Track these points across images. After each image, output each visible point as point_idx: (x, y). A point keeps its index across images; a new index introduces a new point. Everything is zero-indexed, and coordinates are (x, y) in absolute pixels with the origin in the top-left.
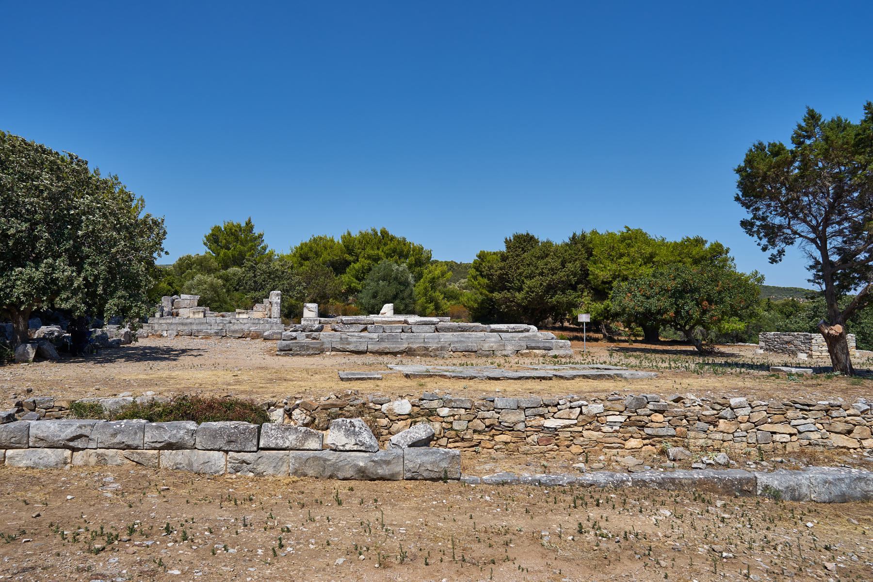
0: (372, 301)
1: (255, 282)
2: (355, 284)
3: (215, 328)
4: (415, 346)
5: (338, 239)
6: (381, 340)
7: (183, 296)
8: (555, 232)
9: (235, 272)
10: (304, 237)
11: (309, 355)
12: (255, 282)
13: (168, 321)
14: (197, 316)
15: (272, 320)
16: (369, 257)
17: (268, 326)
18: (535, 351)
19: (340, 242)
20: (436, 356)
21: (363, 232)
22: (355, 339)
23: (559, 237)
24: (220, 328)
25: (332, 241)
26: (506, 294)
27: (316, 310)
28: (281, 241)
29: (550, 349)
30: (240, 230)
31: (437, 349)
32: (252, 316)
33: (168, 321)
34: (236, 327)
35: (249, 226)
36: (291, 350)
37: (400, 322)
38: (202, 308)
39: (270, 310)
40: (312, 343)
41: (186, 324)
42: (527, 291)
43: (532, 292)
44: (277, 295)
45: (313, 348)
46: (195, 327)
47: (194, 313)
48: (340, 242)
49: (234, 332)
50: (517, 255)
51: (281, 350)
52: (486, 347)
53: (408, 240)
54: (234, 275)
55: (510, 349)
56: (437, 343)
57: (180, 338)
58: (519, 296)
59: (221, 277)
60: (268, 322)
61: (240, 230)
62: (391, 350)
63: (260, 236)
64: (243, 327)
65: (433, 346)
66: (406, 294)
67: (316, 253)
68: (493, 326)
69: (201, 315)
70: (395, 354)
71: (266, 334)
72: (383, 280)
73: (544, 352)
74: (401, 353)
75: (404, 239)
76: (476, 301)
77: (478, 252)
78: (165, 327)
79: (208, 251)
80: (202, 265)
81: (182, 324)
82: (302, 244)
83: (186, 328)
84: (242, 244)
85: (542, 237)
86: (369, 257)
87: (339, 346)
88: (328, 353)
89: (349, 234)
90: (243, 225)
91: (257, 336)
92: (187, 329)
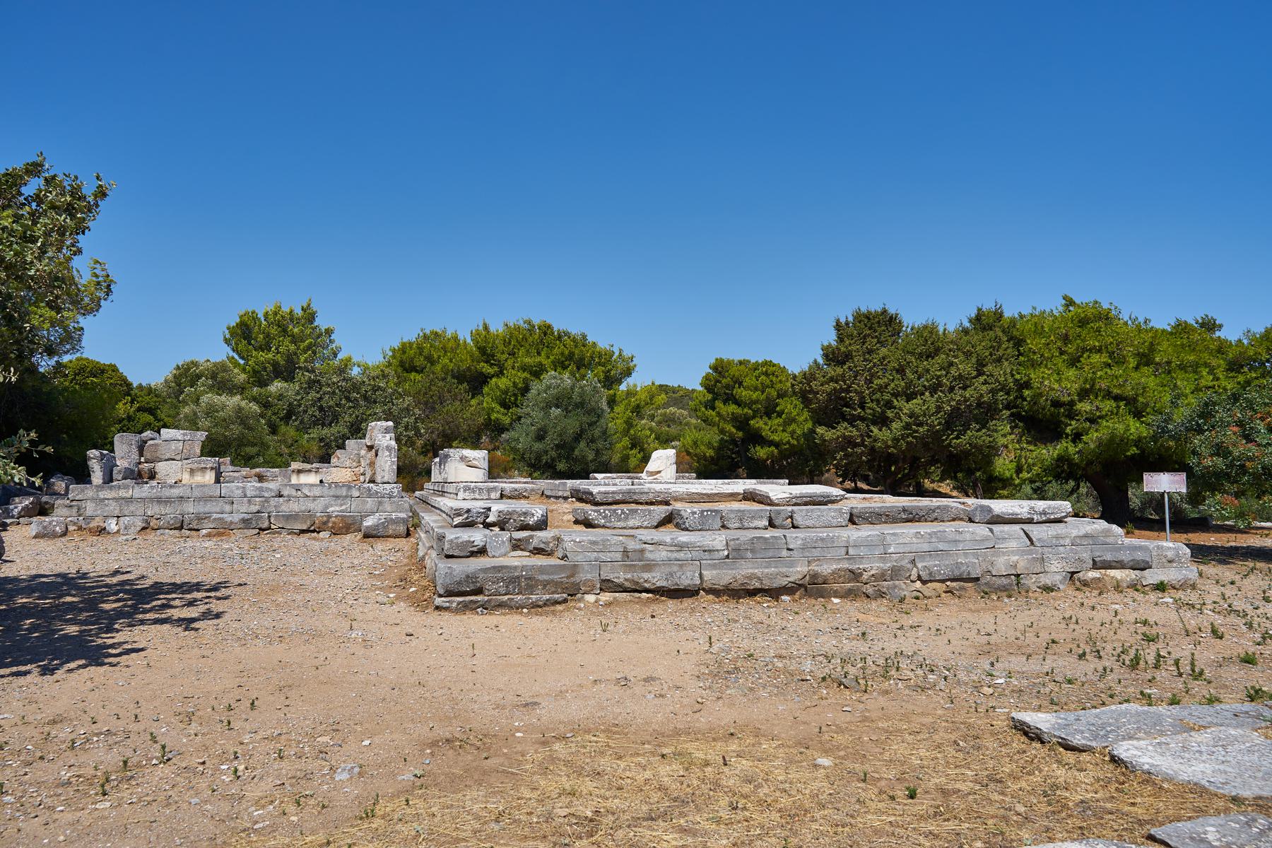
0: (538, 446)
1: (321, 409)
2: (499, 415)
3: (243, 510)
4: (826, 569)
5: (465, 336)
6: (735, 553)
7: (166, 433)
8: (937, 304)
9: (279, 401)
10: (406, 330)
11: (535, 606)
12: (321, 409)
13: (122, 493)
14: (199, 478)
15: (380, 488)
16: (524, 368)
17: (370, 503)
18: (1112, 573)
19: (469, 340)
20: (881, 595)
21: (511, 325)
22: (662, 554)
23: (951, 317)
24: (254, 508)
25: (456, 339)
26: (843, 429)
27: (486, 465)
28: (364, 341)
29: (1142, 567)
30: (292, 320)
31: (882, 576)
32: (327, 479)
33: (122, 493)
34: (294, 507)
35: (310, 317)
36: (479, 591)
37: (733, 496)
38: (211, 461)
39: (372, 464)
40: (542, 569)
41: (167, 501)
42: (885, 422)
43: (921, 425)
44: (387, 431)
45: (545, 584)
46: (190, 508)
47: (192, 471)
48: (469, 340)
49: (289, 518)
50: (870, 352)
51: (450, 593)
52: (1001, 565)
53: (590, 339)
54: (280, 397)
55: (1055, 570)
56: (883, 560)
57: (152, 536)
58: (882, 435)
59: (254, 399)
60: (370, 494)
61: (292, 320)
62: (767, 584)
63: (329, 332)
64: (311, 506)
65: (872, 566)
66: (597, 432)
67: (429, 358)
68: (1000, 506)
69: (210, 477)
70: (774, 593)
71: (369, 522)
72: (557, 407)
73: (1133, 575)
74: (789, 590)
75: (584, 337)
76: (709, 445)
77: (713, 361)
78: (113, 508)
79: (231, 354)
80: (219, 380)
81: (159, 500)
82: (404, 345)
83: (168, 509)
84: (294, 342)
85: (911, 318)
86: (524, 368)
87: (621, 577)
88: (591, 598)
89: (486, 328)
90: (298, 312)
91: (345, 527)
92: (171, 513)
